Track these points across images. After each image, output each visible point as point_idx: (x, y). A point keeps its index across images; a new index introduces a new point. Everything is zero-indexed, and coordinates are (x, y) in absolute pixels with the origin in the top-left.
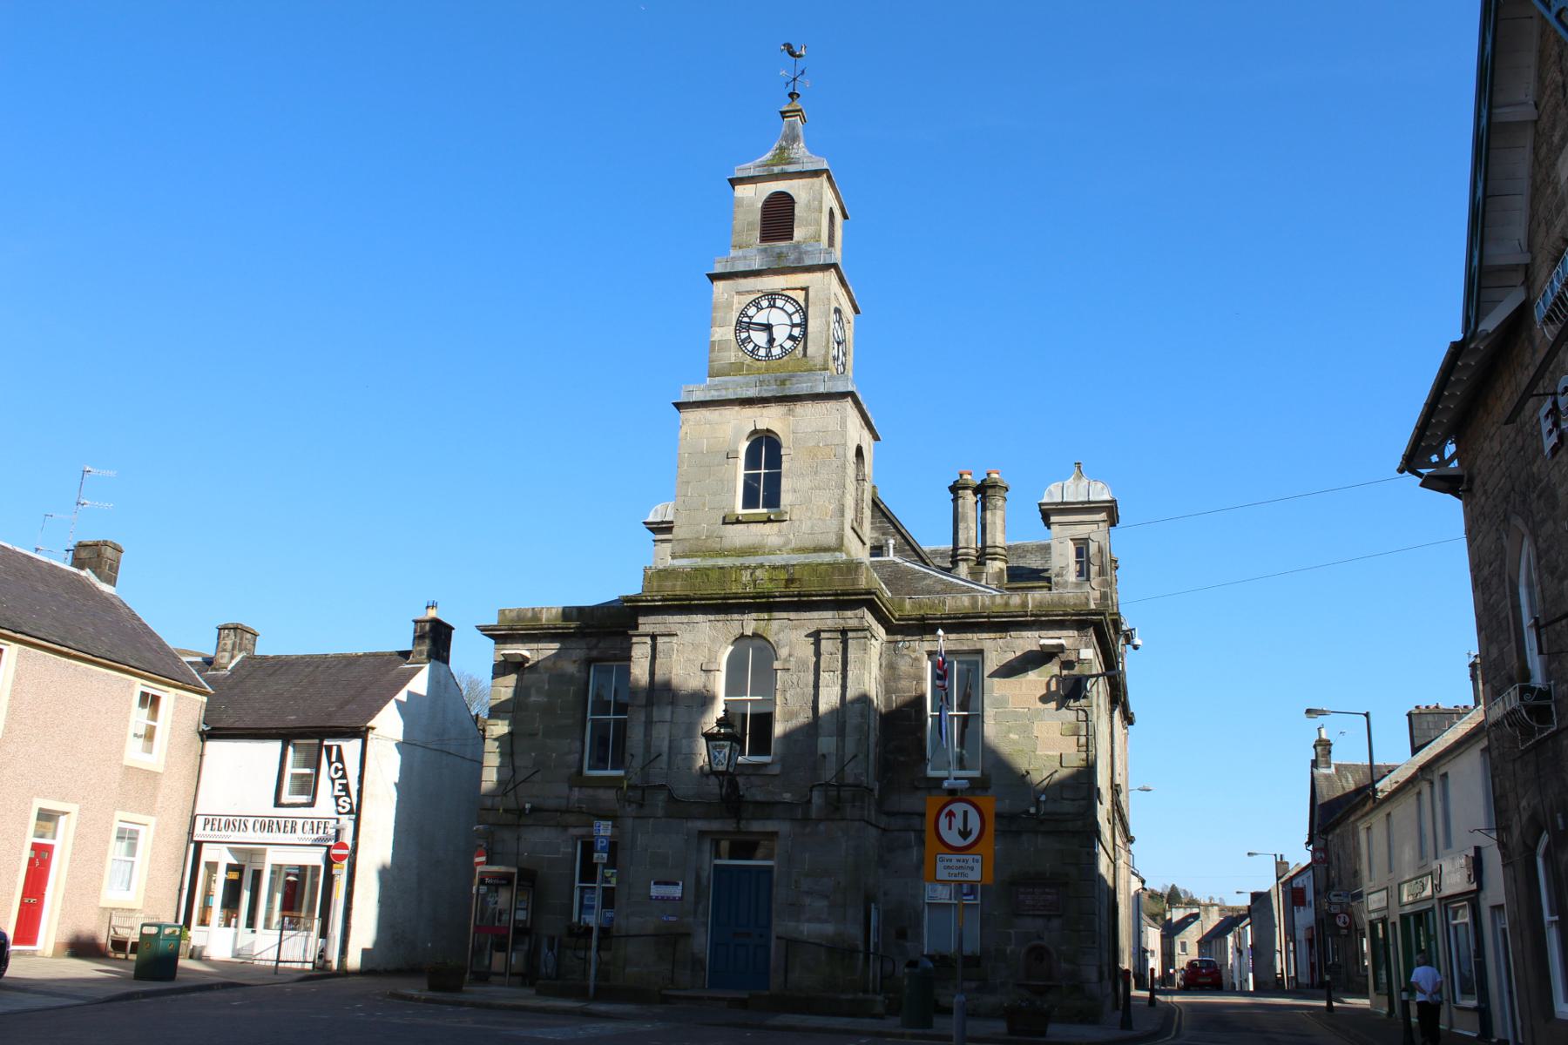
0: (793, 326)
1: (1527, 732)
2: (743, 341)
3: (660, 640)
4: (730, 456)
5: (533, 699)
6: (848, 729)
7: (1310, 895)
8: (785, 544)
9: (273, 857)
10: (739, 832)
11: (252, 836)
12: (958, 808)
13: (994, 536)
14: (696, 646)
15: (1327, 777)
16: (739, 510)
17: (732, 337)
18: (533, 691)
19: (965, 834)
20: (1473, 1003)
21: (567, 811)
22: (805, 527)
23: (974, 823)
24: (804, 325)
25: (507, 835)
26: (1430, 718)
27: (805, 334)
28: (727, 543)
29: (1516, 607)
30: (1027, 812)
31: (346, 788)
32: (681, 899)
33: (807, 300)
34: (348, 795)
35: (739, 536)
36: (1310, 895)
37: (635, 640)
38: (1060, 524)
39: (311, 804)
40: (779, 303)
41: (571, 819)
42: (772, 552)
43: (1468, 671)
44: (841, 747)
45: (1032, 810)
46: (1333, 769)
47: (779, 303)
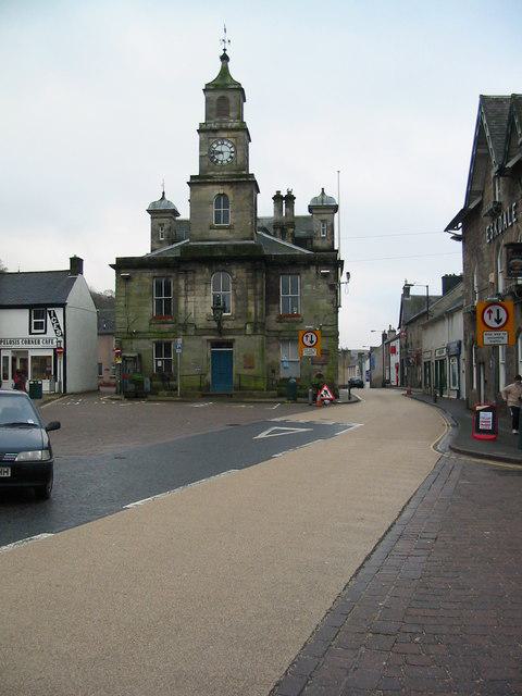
7: (398, 350)
9: (31, 353)
11: (21, 346)
19: (312, 342)
25: (126, 342)
27: (236, 156)
31: (58, 326)
35: (214, 234)
36: (398, 350)
39: (45, 333)
44: (256, 311)
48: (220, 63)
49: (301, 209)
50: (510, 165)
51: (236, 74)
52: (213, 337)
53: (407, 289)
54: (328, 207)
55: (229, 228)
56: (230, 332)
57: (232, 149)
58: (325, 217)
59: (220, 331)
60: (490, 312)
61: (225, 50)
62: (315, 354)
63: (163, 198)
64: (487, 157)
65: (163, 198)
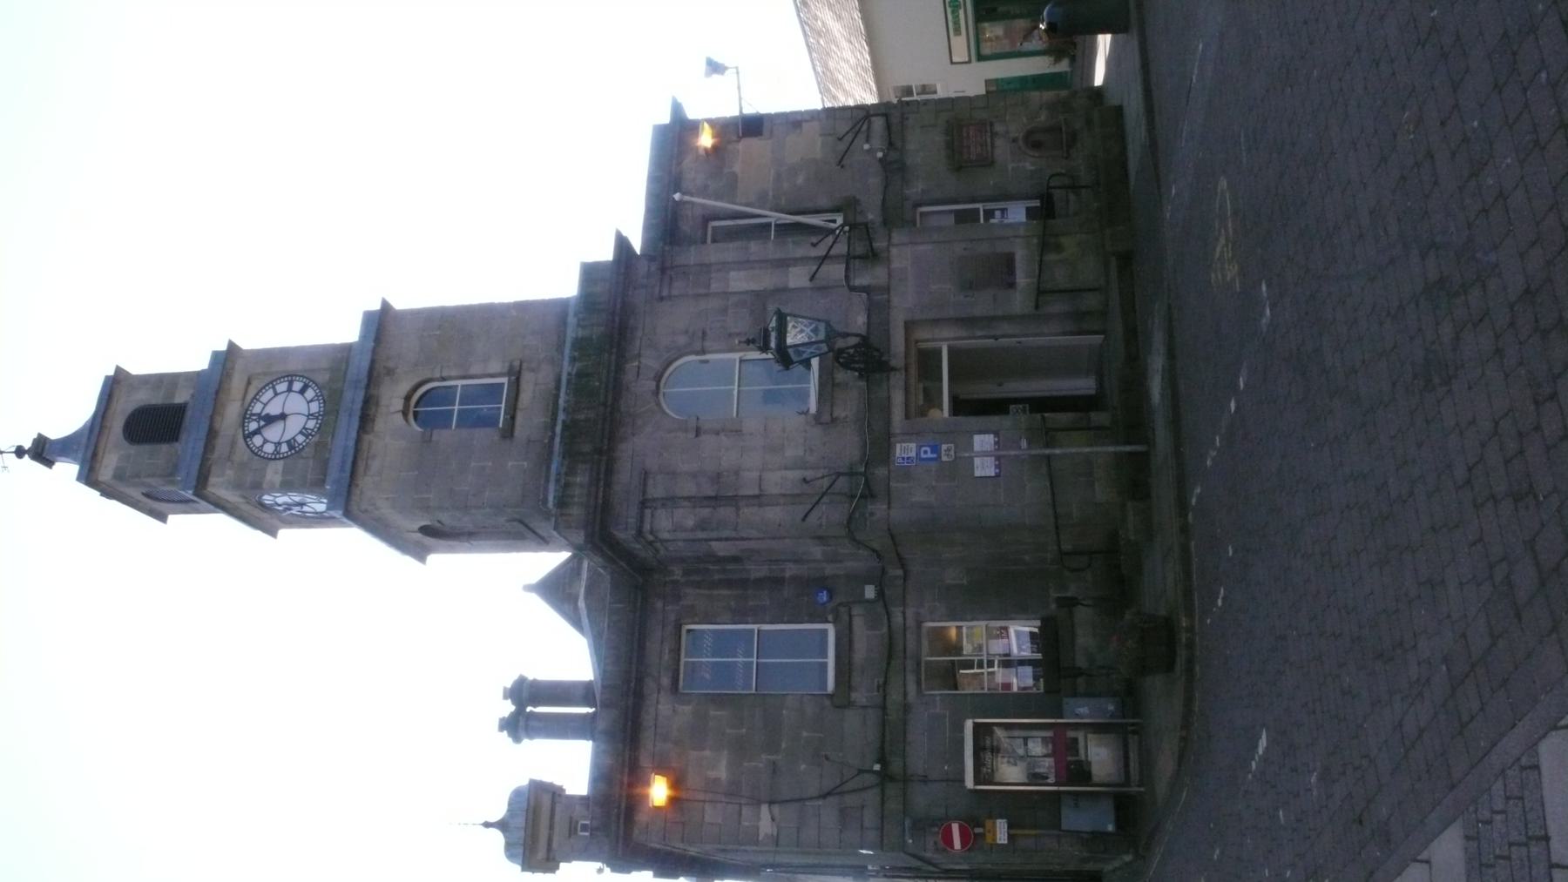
2: (291, 447)
18: (712, 774)
21: (884, 708)
24: (290, 377)
41: (895, 696)
45: (880, 155)
57: (282, 387)
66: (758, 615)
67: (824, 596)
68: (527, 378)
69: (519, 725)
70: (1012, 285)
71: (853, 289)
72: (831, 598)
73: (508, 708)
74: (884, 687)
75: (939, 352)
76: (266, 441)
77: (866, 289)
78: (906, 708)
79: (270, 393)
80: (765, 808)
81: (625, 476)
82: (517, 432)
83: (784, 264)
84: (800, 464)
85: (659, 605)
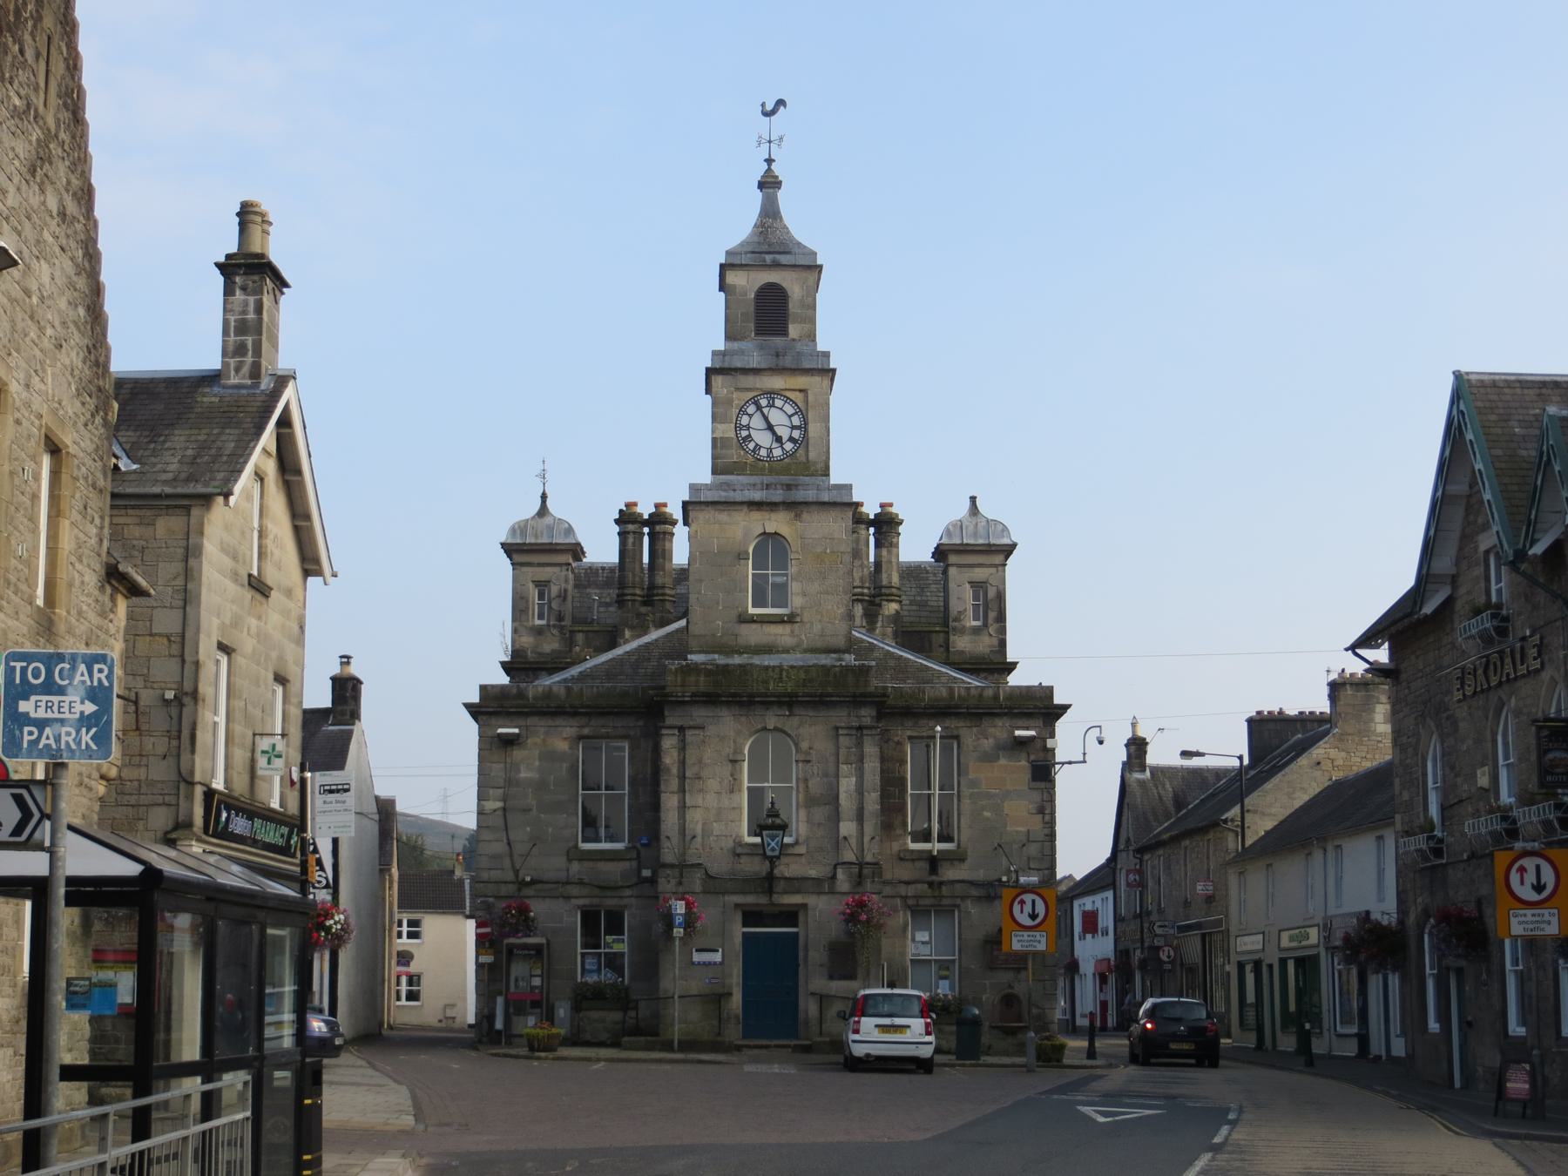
0: (793, 428)
1: (1426, 859)
2: (745, 439)
3: (689, 733)
4: (741, 556)
5: (522, 775)
6: (866, 813)
8: (798, 645)
10: (773, 904)
12: (1028, 898)
13: (890, 576)
14: (722, 738)
15: (1141, 783)
16: (752, 611)
17: (733, 435)
18: (522, 768)
19: (1033, 916)
20: (1355, 1030)
21: (568, 883)
22: (817, 627)
23: (1040, 908)
24: (804, 427)
26: (1271, 726)
28: (741, 641)
29: (1425, 775)
30: (1000, 880)
32: (722, 963)
33: (806, 402)
34: (322, 869)
37: (664, 732)
38: (959, 566)
40: (778, 403)
41: (574, 890)
42: (786, 651)
43: (1326, 690)
45: (1004, 879)
46: (1148, 773)
47: (778, 403)
48: (758, 196)
49: (915, 547)
50: (1538, 549)
51: (800, 223)
52: (750, 899)
53: (1137, 747)
54: (990, 549)
55: (791, 619)
56: (797, 884)
57: (796, 421)
58: (980, 574)
59: (768, 883)
60: (1522, 870)
61: (769, 161)
62: (1042, 947)
63: (543, 511)
64: (1472, 503)
65: (543, 511)
66: (633, 794)
67: (645, 841)
68: (787, 629)
69: (627, 519)
70: (831, 977)
71: (835, 867)
72: (643, 845)
73: (645, 510)
74: (581, 883)
75: (796, 925)
76: (750, 416)
77: (834, 877)
78: (568, 898)
79: (790, 410)
80: (499, 804)
81: (700, 714)
82: (743, 626)
83: (860, 817)
84: (706, 832)
85: (641, 723)
